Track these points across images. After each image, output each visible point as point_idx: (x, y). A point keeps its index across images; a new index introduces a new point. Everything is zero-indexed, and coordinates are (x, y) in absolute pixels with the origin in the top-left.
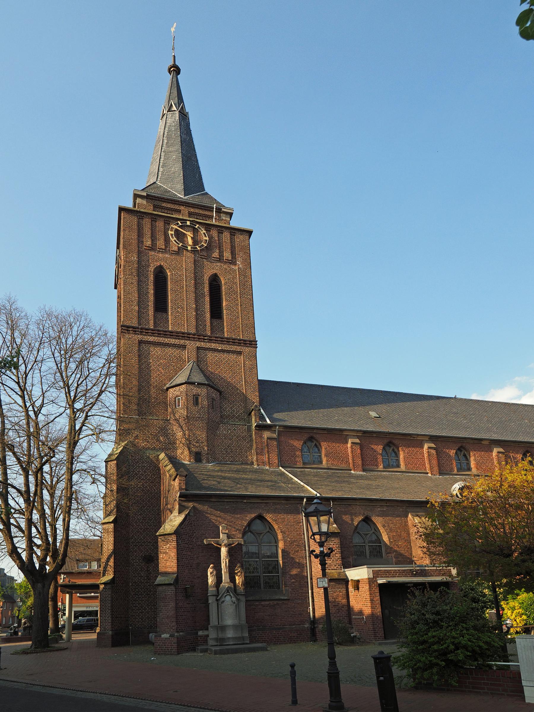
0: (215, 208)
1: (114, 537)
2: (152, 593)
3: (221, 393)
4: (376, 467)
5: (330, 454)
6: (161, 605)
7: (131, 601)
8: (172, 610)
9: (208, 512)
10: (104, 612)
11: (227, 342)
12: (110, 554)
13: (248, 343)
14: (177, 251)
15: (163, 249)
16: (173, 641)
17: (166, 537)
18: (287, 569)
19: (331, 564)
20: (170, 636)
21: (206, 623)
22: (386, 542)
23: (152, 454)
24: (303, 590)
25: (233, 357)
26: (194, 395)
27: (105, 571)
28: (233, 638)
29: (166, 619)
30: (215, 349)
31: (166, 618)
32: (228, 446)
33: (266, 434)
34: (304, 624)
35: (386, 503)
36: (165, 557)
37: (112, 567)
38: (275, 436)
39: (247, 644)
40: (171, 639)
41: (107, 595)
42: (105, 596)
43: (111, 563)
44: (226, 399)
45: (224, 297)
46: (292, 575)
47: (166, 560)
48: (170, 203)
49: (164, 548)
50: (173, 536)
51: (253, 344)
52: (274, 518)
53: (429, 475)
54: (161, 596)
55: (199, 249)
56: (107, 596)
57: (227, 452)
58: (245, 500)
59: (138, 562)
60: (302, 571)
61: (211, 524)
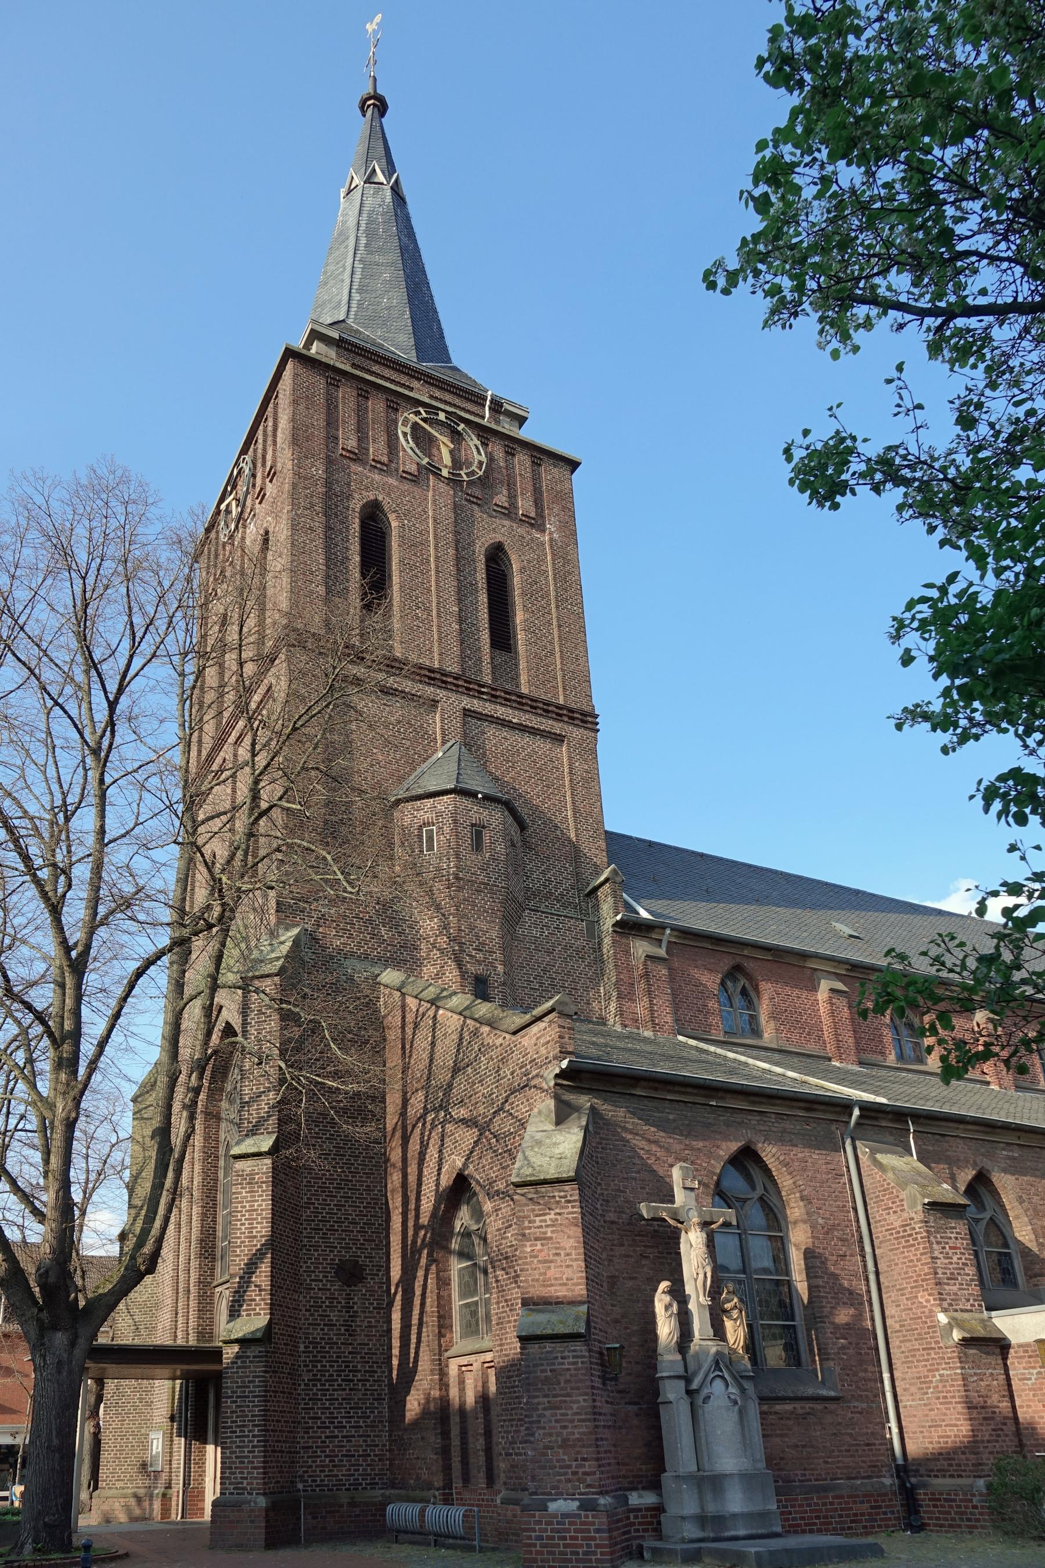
0: (489, 398)
1: (272, 1200)
2: (359, 1377)
3: (522, 826)
4: (880, 1058)
5: (781, 1013)
6: (539, 1404)
7: (304, 1399)
8: (580, 1420)
9: (627, 1125)
10: (235, 1432)
11: (532, 707)
12: (258, 1250)
13: (578, 718)
14: (416, 473)
15: (383, 464)
16: (593, 1524)
17: (542, 1189)
18: (824, 1307)
19: (956, 1294)
20: (580, 1508)
21: (644, 1467)
22: (1029, 1245)
23: (359, 972)
24: (866, 1371)
25: (542, 746)
26: (473, 825)
27: (239, 1301)
28: (744, 1515)
29: (561, 1451)
30: (504, 720)
31: (560, 1447)
32: (544, 970)
33: (640, 948)
34: (881, 1476)
35: (1019, 1138)
36: (541, 1251)
37: (265, 1290)
38: (662, 952)
39: (777, 1535)
40: (587, 1516)
41: (248, 1377)
42: (243, 1382)
43: (263, 1276)
44: (531, 849)
45: (518, 601)
46: (837, 1327)
47: (545, 1262)
48: (389, 367)
49: (538, 1224)
50: (567, 1188)
51: (587, 719)
52: (782, 1158)
53: (994, 1087)
54: (539, 1374)
55: (465, 478)
56: (249, 1382)
57: (541, 984)
58: (712, 1098)
59: (321, 1281)
60: (859, 1316)
61: (636, 1161)
